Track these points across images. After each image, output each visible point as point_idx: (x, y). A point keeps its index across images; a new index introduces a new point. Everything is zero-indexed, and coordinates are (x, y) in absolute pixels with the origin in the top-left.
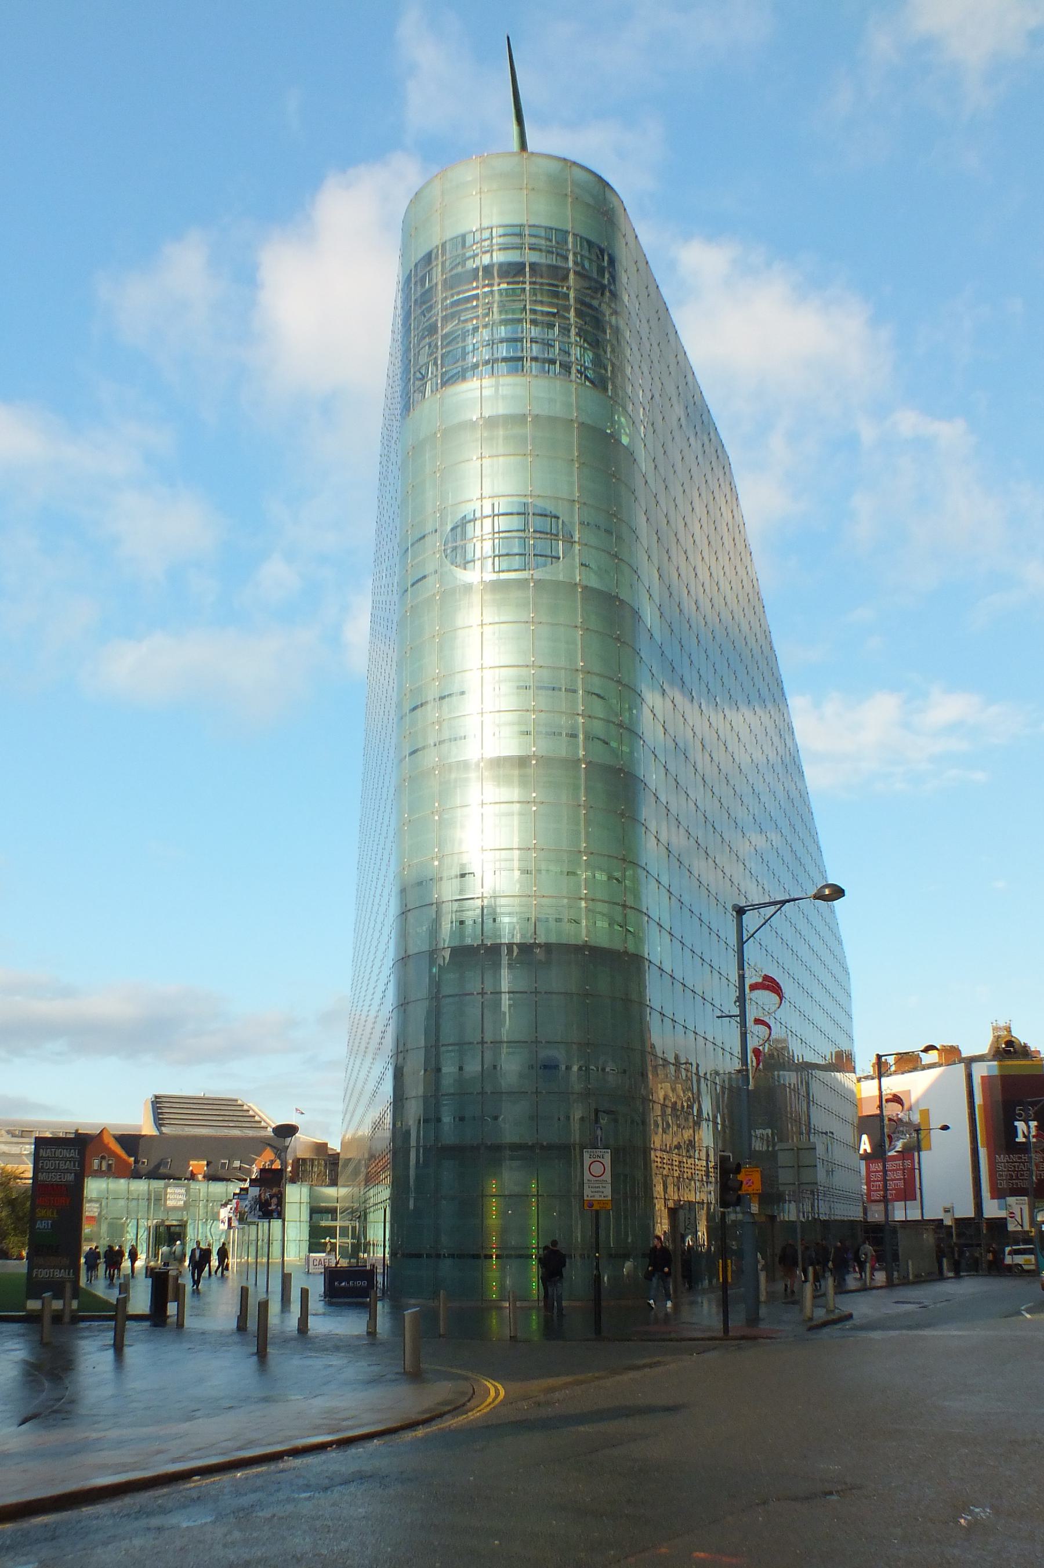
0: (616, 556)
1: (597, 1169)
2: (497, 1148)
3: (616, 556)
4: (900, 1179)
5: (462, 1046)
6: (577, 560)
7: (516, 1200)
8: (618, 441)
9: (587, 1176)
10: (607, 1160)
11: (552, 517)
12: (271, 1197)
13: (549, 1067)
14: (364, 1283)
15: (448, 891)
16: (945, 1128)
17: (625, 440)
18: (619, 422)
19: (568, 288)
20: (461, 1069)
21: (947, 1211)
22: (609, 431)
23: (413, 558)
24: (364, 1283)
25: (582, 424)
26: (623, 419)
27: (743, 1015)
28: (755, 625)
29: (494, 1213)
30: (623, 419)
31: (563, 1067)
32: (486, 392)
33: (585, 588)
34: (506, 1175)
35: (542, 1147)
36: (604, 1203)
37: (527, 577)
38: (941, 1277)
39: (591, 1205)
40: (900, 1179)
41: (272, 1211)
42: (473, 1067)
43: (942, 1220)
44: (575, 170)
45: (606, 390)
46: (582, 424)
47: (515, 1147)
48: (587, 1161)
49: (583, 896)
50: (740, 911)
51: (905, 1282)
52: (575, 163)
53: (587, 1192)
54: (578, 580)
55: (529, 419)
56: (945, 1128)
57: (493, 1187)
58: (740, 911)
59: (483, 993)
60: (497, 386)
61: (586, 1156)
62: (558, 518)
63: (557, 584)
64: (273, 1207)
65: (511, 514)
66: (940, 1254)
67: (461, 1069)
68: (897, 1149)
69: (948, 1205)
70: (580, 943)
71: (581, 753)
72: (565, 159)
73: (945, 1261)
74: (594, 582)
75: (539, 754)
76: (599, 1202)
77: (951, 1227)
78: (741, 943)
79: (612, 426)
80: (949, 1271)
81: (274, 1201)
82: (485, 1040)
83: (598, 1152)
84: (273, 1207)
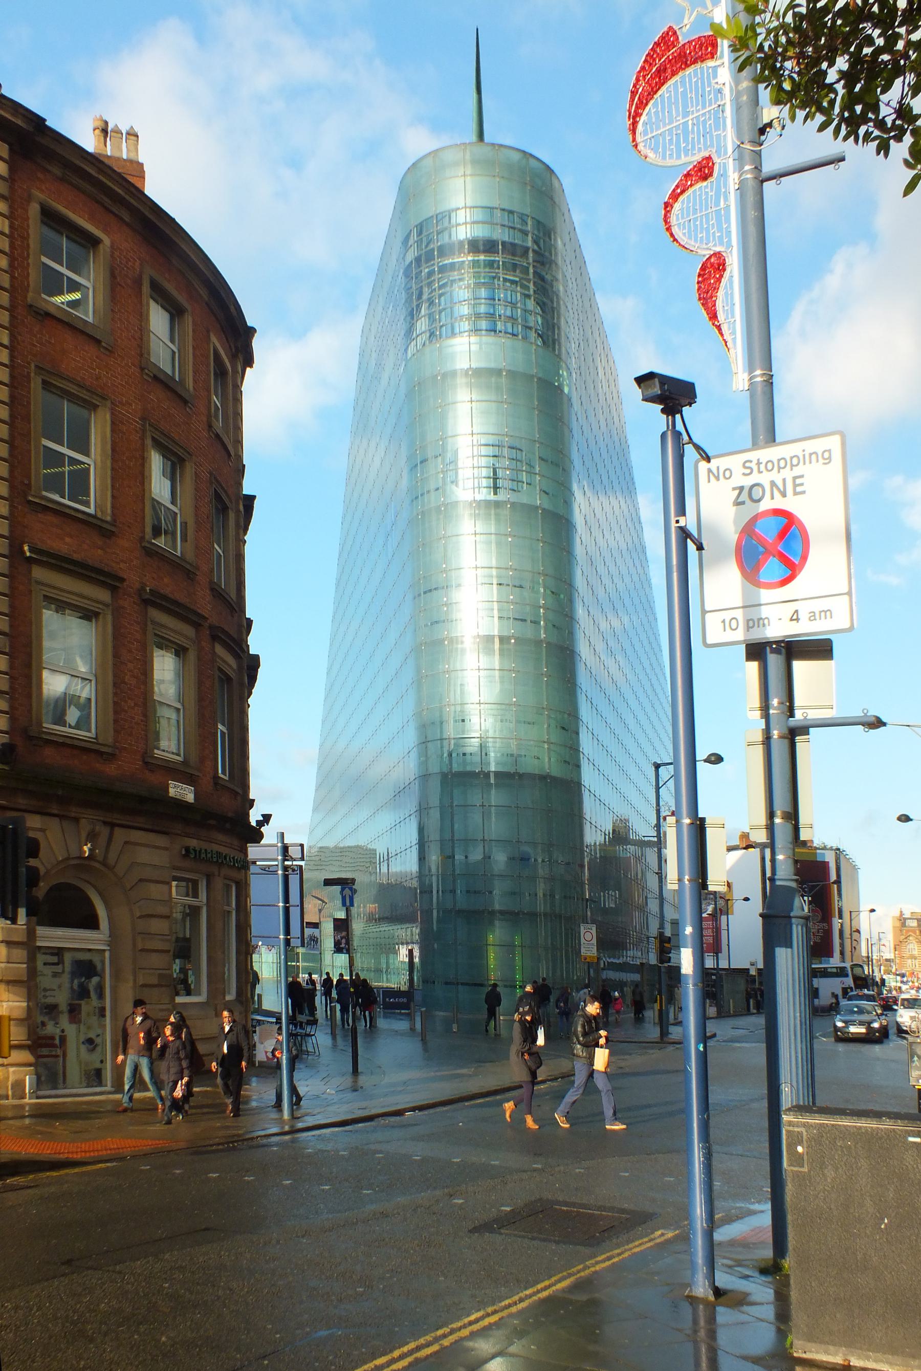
0: (562, 484)
2: (492, 913)
3: (562, 484)
4: (710, 936)
5: (468, 842)
6: (538, 488)
7: (509, 947)
8: (562, 391)
9: (583, 940)
10: (594, 931)
11: (517, 449)
12: (342, 938)
13: (524, 859)
14: (405, 1000)
15: (450, 731)
16: (747, 899)
17: (566, 390)
18: (562, 376)
19: (528, 263)
20: (466, 857)
21: (752, 964)
22: (556, 384)
23: (422, 474)
24: (405, 1000)
26: (565, 373)
27: (851, 938)
28: (632, 510)
29: (492, 957)
30: (565, 373)
31: (533, 860)
32: (473, 347)
33: (544, 510)
34: (497, 931)
35: (524, 914)
36: (593, 957)
38: (748, 1013)
39: (586, 959)
40: (710, 936)
41: (343, 948)
43: (748, 969)
44: (532, 161)
45: (554, 350)
46: (539, 379)
48: (582, 931)
49: (546, 740)
50: (657, 766)
53: (583, 950)
54: (538, 502)
56: (747, 899)
57: (491, 937)
58: (657, 766)
59: (483, 806)
60: (480, 344)
61: (582, 928)
62: (522, 450)
63: (523, 505)
64: (343, 945)
66: (748, 996)
68: (708, 912)
69: (753, 960)
70: (544, 774)
72: (524, 152)
77: (755, 976)
78: (658, 788)
79: (559, 379)
81: (344, 941)
83: (589, 926)
84: (343, 945)
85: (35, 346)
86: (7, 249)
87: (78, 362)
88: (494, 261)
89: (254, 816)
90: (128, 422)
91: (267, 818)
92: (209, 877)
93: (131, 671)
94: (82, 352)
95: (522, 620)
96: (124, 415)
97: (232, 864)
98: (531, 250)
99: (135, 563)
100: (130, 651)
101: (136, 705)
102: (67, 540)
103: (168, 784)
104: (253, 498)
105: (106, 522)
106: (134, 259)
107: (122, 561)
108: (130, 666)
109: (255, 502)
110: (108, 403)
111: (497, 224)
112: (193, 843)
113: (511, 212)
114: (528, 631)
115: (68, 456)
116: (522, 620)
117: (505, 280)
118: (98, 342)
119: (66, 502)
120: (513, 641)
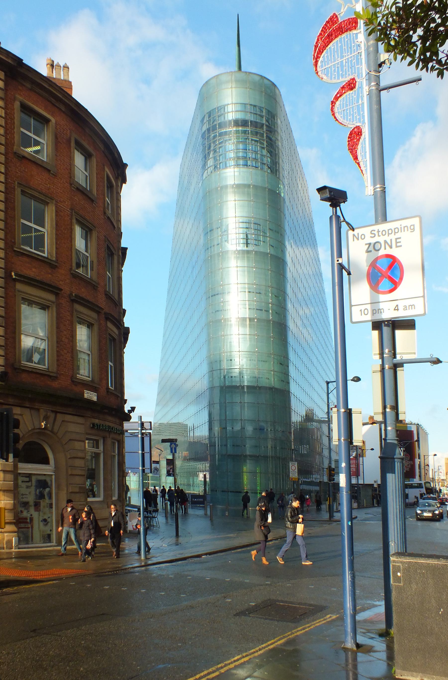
0: (280, 242)
1: (293, 468)
3: (280, 242)
4: (354, 468)
5: (233, 421)
7: (253, 473)
8: (280, 195)
9: (291, 470)
12: (170, 469)
13: (261, 429)
14: (202, 500)
16: (372, 449)
17: (282, 195)
18: (280, 188)
20: (233, 428)
21: (375, 482)
22: (277, 192)
24: (202, 500)
25: (269, 189)
26: (282, 187)
29: (246, 478)
33: (271, 255)
36: (296, 478)
37: (252, 250)
40: (354, 468)
41: (171, 474)
42: (238, 427)
45: (276, 175)
47: (250, 456)
48: (290, 465)
50: (328, 383)
51: (363, 507)
52: (265, 77)
53: (291, 475)
55: (252, 187)
56: (372, 449)
58: (328, 383)
59: (241, 403)
63: (261, 253)
64: (171, 472)
65: (244, 222)
66: (373, 498)
67: (233, 428)
69: (376, 480)
70: (271, 387)
71: (271, 318)
72: (261, 76)
73: (375, 500)
74: (272, 253)
75: (258, 317)
76: (294, 478)
78: (328, 394)
79: (279, 189)
80: (376, 504)
81: (171, 470)
82: (242, 419)
83: (294, 463)
84: (171, 472)
85: (18, 173)
86: (3, 125)
87: (39, 181)
88: (246, 131)
89: (127, 408)
90: (64, 211)
91: (133, 409)
92: (104, 438)
93: (65, 335)
94: (41, 176)
95: (260, 310)
96: (62, 207)
97: (116, 432)
98: (265, 125)
99: (67, 281)
100: (65, 325)
101: (68, 352)
102: (34, 270)
103: (84, 392)
104: (126, 400)
105: (53, 261)
106: (67, 129)
107: (61, 280)
108: (65, 333)
109: (127, 251)
110: (54, 202)
111: (248, 112)
112: (96, 421)
113: (255, 106)
114: (264, 315)
115: (34, 228)
116: (260, 310)
117: (252, 140)
118: (49, 171)
119: (33, 251)
120: (256, 320)
